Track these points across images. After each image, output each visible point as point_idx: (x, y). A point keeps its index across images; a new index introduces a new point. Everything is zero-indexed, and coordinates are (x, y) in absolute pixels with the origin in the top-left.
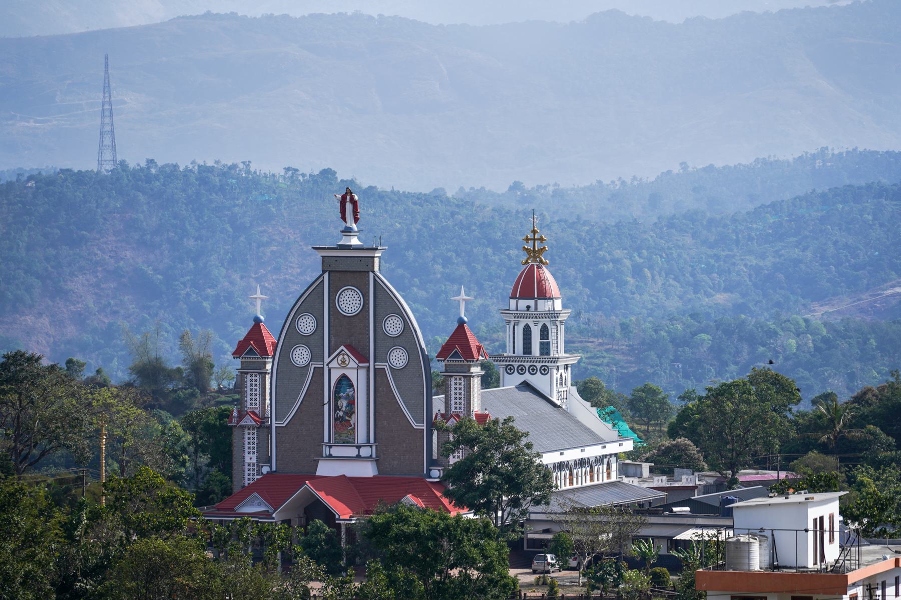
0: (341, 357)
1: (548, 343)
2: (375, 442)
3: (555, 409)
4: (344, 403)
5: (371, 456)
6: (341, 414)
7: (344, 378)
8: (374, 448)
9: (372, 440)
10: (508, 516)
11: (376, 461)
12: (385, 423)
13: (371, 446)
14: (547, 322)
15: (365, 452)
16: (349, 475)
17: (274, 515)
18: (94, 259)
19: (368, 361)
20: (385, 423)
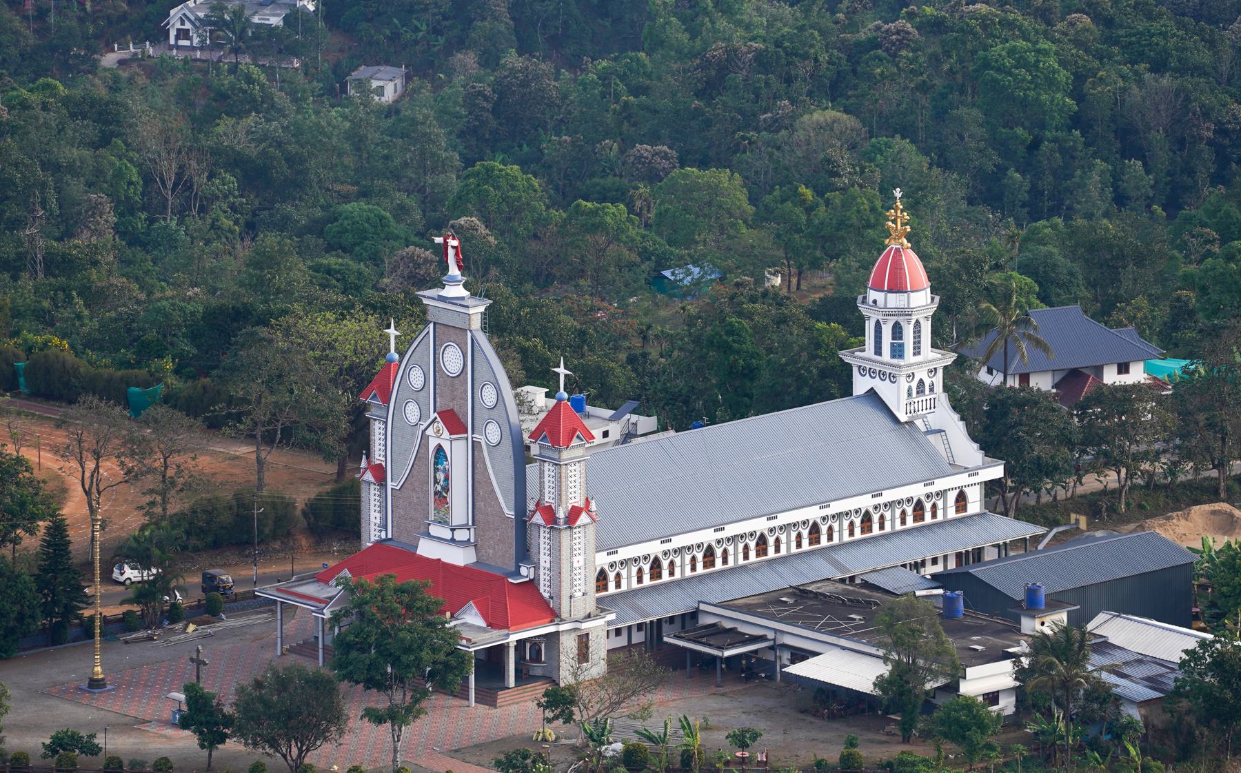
0: (436, 424)
1: (902, 345)
2: (473, 524)
3: (896, 427)
4: (441, 476)
5: (469, 540)
6: (439, 488)
7: (439, 449)
8: (472, 530)
9: (470, 523)
10: (757, 580)
11: (475, 546)
12: (482, 504)
13: (469, 529)
14: (900, 319)
15: (461, 535)
16: (444, 560)
17: (325, 611)
18: (660, 51)
19: (467, 432)
20: (482, 504)
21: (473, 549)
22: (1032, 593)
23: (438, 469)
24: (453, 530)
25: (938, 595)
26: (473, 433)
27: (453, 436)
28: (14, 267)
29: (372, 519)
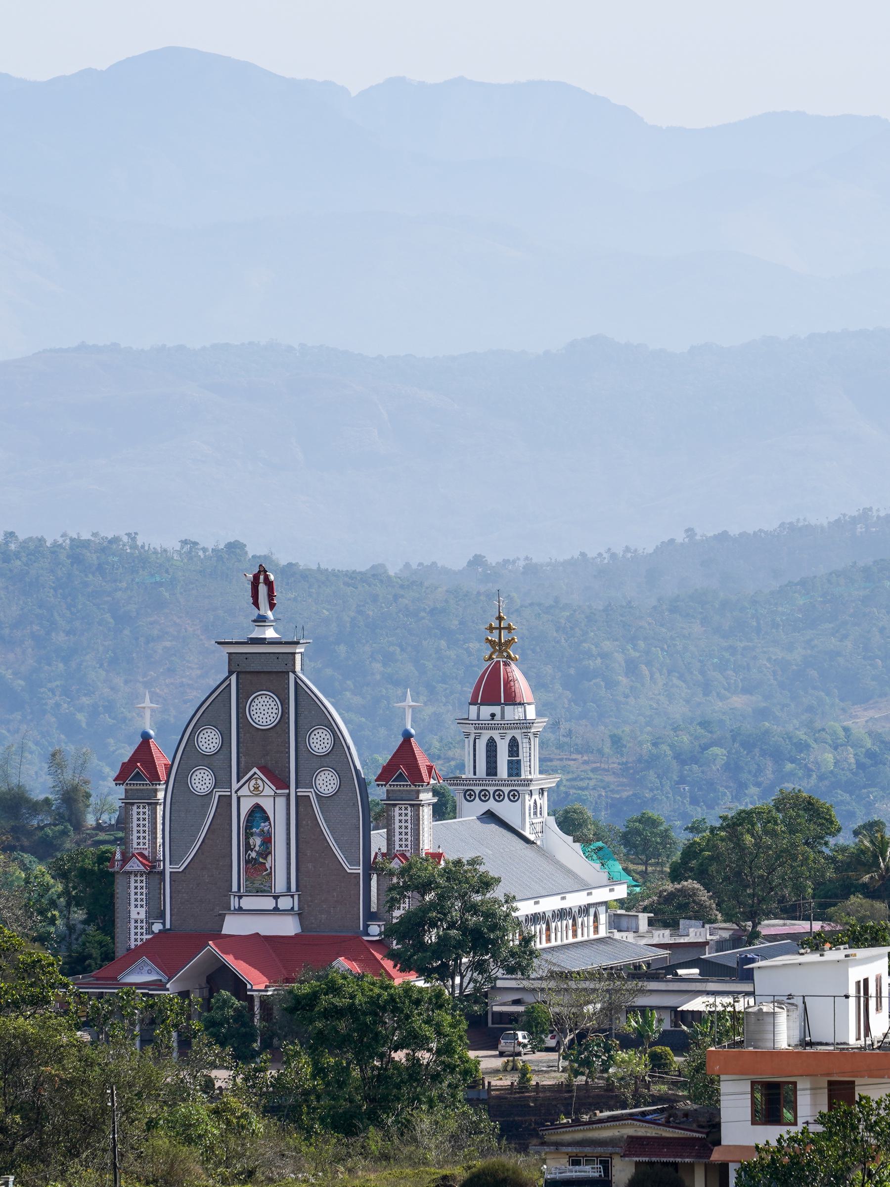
0: (253, 782)
1: (519, 762)
2: (297, 890)
4: (257, 841)
5: (293, 908)
6: (254, 855)
8: (296, 897)
11: (299, 914)
13: (292, 896)
19: (288, 787)
20: (310, 866)
21: (297, 918)
22: (514, 897)
23: (252, 834)
24: (276, 898)
25: (378, 881)
26: (297, 788)
27: (278, 791)
28: (841, 1177)
29: (134, 915)
